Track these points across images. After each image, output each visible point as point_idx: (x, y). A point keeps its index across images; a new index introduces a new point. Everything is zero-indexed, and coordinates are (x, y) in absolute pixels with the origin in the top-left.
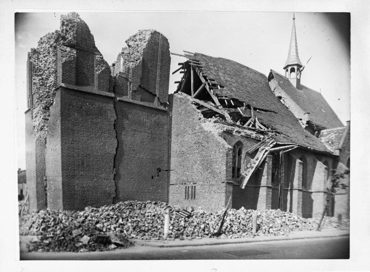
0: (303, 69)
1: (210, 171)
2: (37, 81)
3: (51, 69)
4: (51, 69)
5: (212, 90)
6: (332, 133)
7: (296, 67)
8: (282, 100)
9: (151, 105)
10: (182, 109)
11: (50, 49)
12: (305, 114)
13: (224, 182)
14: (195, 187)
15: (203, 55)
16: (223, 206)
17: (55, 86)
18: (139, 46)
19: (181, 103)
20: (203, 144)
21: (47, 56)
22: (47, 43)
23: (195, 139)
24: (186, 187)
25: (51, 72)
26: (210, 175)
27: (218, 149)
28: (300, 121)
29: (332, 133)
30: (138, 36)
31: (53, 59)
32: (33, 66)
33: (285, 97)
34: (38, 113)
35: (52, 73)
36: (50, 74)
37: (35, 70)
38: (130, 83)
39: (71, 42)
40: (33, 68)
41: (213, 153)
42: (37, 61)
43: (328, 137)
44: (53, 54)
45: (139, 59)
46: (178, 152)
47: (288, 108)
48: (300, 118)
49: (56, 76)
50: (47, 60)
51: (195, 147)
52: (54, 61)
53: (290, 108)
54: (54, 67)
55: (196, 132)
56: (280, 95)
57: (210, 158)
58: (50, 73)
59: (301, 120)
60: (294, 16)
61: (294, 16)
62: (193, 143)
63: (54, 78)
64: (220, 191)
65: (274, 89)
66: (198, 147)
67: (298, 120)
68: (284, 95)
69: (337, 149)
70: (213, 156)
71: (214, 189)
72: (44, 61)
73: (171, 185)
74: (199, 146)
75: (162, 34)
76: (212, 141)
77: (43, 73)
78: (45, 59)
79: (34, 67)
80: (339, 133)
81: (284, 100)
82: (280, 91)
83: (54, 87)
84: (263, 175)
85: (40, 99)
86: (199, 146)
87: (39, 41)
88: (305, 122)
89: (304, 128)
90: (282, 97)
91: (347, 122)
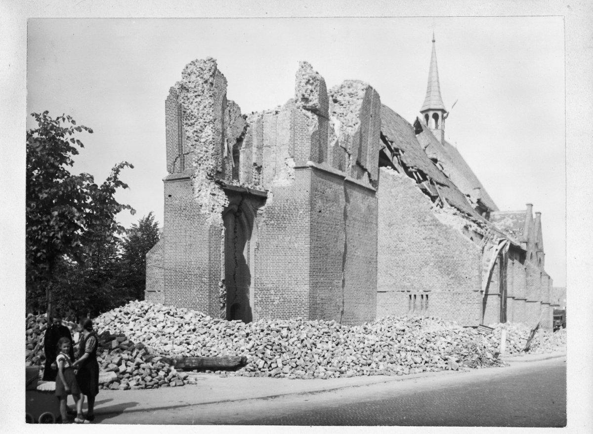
0: (447, 115)
1: (452, 275)
2: (191, 134)
3: (206, 116)
4: (206, 116)
5: (395, 157)
6: (507, 218)
7: (440, 113)
8: (437, 165)
9: (358, 182)
10: (398, 190)
11: (205, 85)
12: (475, 189)
13: (477, 291)
14: (427, 296)
15: (398, 115)
16: (476, 320)
17: (213, 143)
18: (351, 103)
19: (395, 182)
20: (439, 241)
21: (199, 95)
22: (199, 76)
23: (424, 233)
24: (410, 296)
25: (208, 121)
26: (452, 281)
27: (466, 249)
28: (468, 198)
29: (507, 218)
30: (346, 88)
31: (209, 101)
32: (183, 110)
33: (443, 160)
34: (202, 185)
35: (209, 122)
36: (206, 124)
37: (186, 116)
38: (349, 155)
39: (316, 106)
40: (183, 113)
41: (457, 253)
42: (187, 102)
43: (502, 222)
44: (209, 95)
45: (357, 124)
46: (393, 248)
47: (449, 177)
48: (467, 194)
49: (214, 128)
50: (201, 102)
51: (425, 243)
52: (211, 104)
53: (451, 177)
54: (211, 114)
55: (426, 223)
56: (435, 157)
57: (452, 259)
58: (205, 122)
59: (468, 196)
60: (434, 37)
61: (434, 37)
62: (421, 238)
63: (212, 131)
64: (471, 302)
65: (426, 148)
66: (430, 244)
67: (465, 197)
68: (441, 158)
69: (524, 242)
70: (457, 258)
71: (460, 299)
72: (197, 104)
73: (490, 295)
74: (432, 243)
75: (375, 90)
76: (455, 238)
77: (196, 121)
78: (199, 99)
79: (185, 112)
80: (518, 219)
81: (441, 164)
82: (436, 152)
83: (211, 143)
84: (492, 280)
85: (199, 162)
86: (432, 243)
87: (182, 71)
88: (475, 201)
89: (474, 208)
90: (439, 159)
91: (527, 205)
